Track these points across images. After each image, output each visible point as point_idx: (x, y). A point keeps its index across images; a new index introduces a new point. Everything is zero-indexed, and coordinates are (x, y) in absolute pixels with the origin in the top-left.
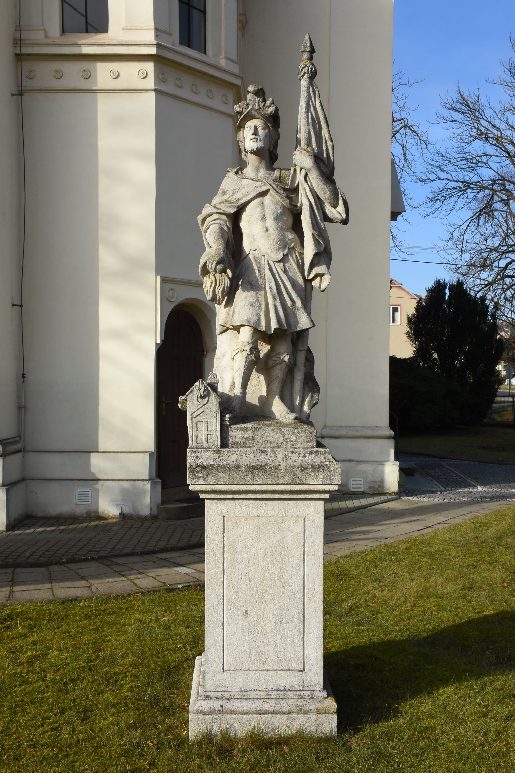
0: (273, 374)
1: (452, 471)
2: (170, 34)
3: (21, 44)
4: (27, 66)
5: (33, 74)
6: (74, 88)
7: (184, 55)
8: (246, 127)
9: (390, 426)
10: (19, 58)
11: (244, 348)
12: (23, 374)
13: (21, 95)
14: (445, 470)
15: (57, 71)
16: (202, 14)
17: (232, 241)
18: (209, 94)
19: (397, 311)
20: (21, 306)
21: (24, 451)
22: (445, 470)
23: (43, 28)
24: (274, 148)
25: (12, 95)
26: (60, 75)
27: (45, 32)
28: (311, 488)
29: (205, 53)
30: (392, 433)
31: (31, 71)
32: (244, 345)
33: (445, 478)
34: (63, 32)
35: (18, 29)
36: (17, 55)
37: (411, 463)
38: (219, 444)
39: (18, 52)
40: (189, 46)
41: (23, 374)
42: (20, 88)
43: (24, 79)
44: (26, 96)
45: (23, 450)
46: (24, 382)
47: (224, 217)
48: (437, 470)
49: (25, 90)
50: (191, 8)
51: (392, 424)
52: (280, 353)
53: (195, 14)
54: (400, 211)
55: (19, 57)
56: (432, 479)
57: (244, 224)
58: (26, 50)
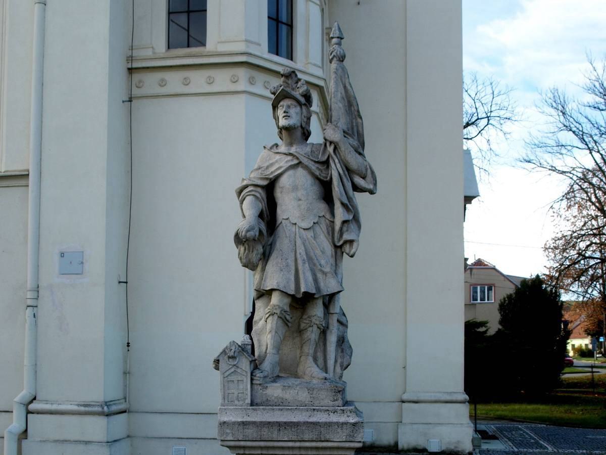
0: (306, 336)
1: (527, 434)
2: (259, 45)
3: (132, 60)
4: (136, 77)
5: (141, 84)
6: (176, 94)
7: (271, 61)
8: (279, 106)
9: (465, 390)
10: (131, 70)
11: (275, 311)
12: (128, 343)
13: (130, 101)
14: (522, 432)
15: (163, 80)
16: (289, 28)
17: (266, 211)
18: (251, 81)
19: (492, 290)
20: (126, 283)
21: (129, 412)
22: (522, 432)
23: (151, 46)
24: (306, 124)
25: (123, 102)
26: (164, 83)
27: (153, 48)
28: (335, 444)
29: (292, 60)
30: (467, 397)
31: (140, 81)
32: (274, 308)
33: (520, 440)
34: (169, 47)
35: (131, 48)
36: (129, 69)
37: (492, 426)
38: (250, 402)
39: (130, 67)
40: (277, 54)
41: (128, 343)
42: (130, 96)
43: (134, 88)
44: (134, 102)
45: (127, 411)
46: (128, 350)
47: (259, 190)
48: (514, 432)
49: (134, 98)
50: (280, 24)
51: (467, 389)
52: (311, 316)
53: (284, 29)
54: (475, 195)
55: (130, 71)
56: (507, 440)
57: (279, 195)
58: (135, 65)
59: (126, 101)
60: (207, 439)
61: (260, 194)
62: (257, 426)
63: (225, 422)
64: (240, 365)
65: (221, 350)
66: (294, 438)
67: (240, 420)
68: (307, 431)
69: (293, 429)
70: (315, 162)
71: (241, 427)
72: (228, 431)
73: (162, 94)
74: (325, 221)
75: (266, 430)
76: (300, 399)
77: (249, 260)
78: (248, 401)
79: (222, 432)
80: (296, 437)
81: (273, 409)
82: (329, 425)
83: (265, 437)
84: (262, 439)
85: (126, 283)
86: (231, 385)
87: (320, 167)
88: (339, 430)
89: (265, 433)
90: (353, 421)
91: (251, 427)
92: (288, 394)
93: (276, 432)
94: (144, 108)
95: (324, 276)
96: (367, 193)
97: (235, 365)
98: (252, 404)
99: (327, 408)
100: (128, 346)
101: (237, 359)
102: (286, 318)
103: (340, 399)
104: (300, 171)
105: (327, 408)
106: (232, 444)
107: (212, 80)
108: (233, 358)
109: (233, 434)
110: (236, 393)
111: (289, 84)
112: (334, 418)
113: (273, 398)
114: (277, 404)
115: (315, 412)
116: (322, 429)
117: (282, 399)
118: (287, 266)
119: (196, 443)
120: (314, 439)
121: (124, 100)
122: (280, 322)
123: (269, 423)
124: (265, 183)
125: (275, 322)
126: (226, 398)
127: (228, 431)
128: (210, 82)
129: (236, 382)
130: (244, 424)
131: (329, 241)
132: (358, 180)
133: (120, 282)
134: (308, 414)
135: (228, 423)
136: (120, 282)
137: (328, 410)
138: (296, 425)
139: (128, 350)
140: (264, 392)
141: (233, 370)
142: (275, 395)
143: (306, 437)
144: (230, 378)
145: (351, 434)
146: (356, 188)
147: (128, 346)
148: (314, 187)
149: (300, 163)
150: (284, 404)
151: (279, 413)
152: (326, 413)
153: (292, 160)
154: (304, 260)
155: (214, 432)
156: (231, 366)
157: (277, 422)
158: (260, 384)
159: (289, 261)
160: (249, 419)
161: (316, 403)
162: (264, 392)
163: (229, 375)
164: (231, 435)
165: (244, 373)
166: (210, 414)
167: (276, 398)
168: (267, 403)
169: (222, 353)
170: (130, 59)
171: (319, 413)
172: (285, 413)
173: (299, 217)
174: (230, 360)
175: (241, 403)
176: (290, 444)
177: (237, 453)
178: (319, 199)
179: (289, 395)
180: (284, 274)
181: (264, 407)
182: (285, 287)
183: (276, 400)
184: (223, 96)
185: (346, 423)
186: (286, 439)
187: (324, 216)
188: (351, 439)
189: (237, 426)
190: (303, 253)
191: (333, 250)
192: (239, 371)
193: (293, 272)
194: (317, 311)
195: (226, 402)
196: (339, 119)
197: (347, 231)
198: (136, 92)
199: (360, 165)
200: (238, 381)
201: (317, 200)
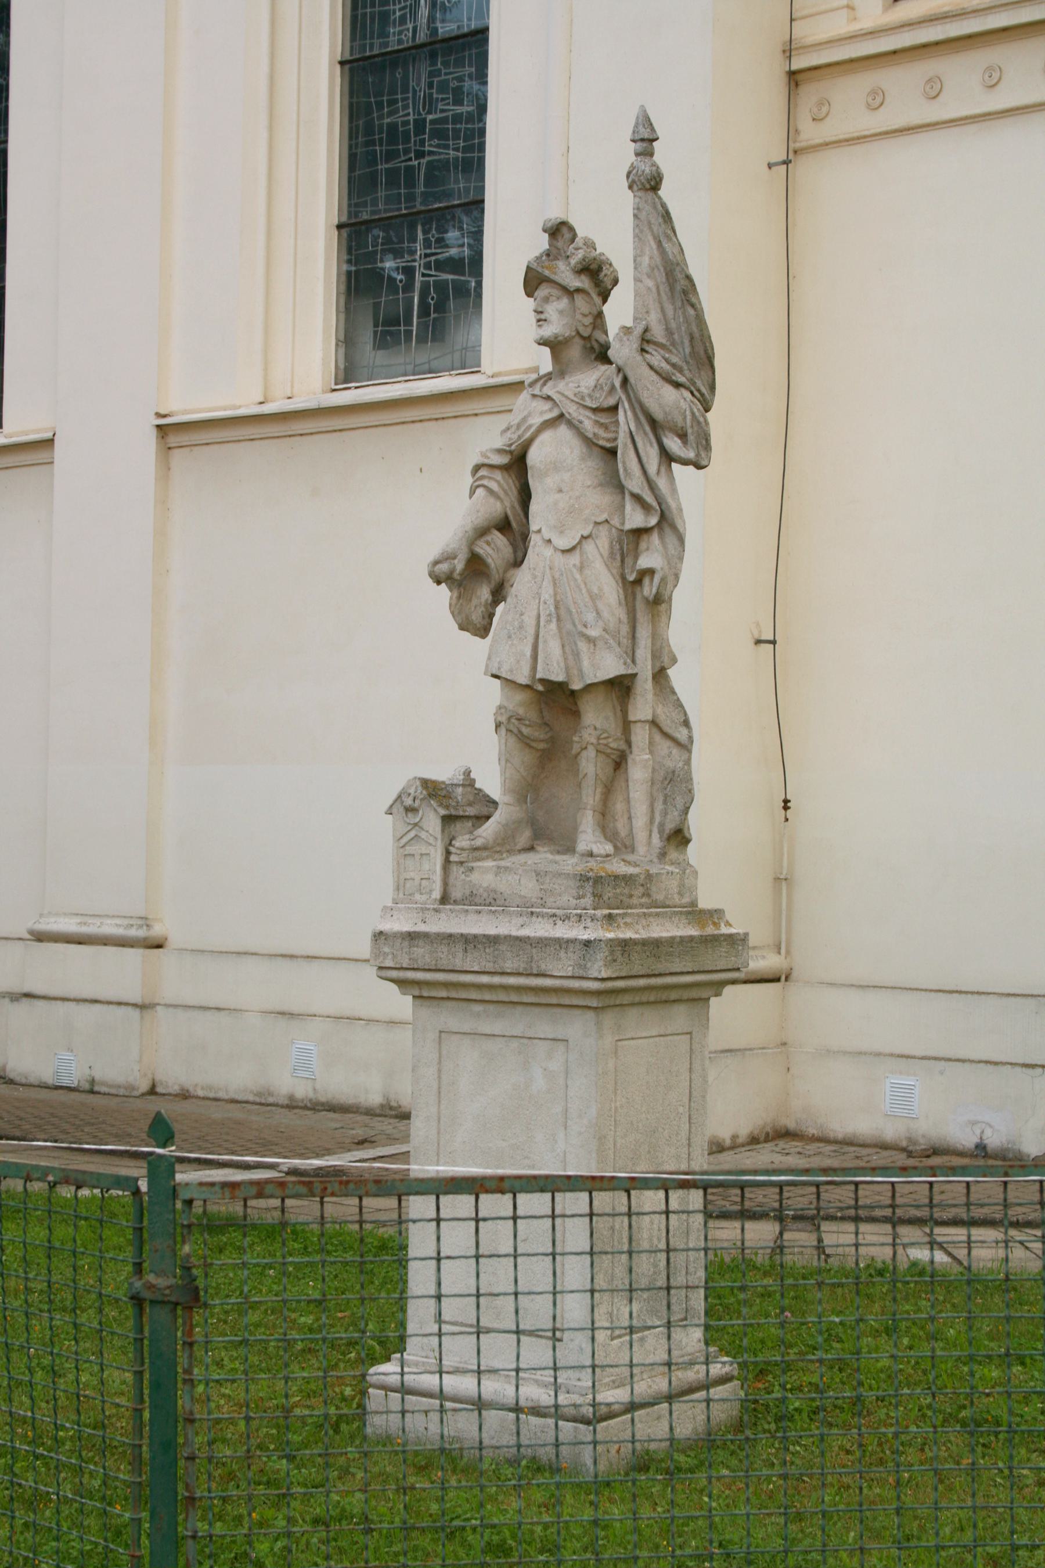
5: (825, 109)
10: (794, 78)
12: (786, 801)
20: (773, 642)
25: (770, 166)
28: (557, 983)
38: (438, 897)
41: (786, 801)
46: (787, 820)
58: (799, 63)
59: (777, 164)
60: (914, 1057)
61: (498, 482)
62: (432, 942)
63: (381, 933)
64: (424, 824)
65: (394, 796)
66: (490, 967)
67: (407, 927)
68: (509, 954)
69: (487, 950)
70: (595, 410)
71: (406, 943)
72: (386, 950)
73: (872, 131)
74: (610, 531)
75: (445, 949)
76: (522, 893)
77: (467, 618)
78: (437, 894)
79: (377, 953)
80: (491, 964)
81: (467, 911)
82: (543, 943)
83: (444, 964)
84: (439, 967)
85: (773, 642)
86: (409, 862)
87: (602, 421)
88: (562, 954)
89: (444, 956)
90: (585, 937)
91: (421, 943)
92: (504, 882)
93: (460, 955)
94: (826, 179)
95: (592, 645)
96: (691, 467)
97: (416, 825)
98: (444, 899)
99: (554, 911)
100: (786, 808)
101: (421, 812)
102: (520, 732)
103: (589, 895)
104: (563, 430)
105: (554, 911)
106: (394, 974)
107: (996, 75)
108: (410, 810)
109: (394, 956)
110: (417, 878)
111: (558, 249)
112: (562, 931)
113: (481, 890)
114: (487, 902)
115: (534, 918)
116: (534, 951)
117: (495, 891)
118: (521, 627)
119: (942, 1073)
120: (521, 970)
121: (773, 161)
122: (512, 740)
123: (450, 936)
124: (504, 460)
125: (503, 741)
126: (401, 888)
127: (386, 950)
128: (934, 91)
129: (417, 857)
130: (412, 937)
131: (612, 575)
132: (673, 444)
133: (758, 642)
134: (521, 920)
135: (386, 934)
136: (758, 642)
137: (554, 915)
138: (493, 940)
139: (787, 820)
140: (468, 879)
141: (412, 834)
142: (485, 885)
143: (509, 966)
144: (409, 849)
145: (582, 962)
146: (667, 457)
147: (786, 808)
148: (589, 463)
149: (562, 416)
150: (498, 902)
151: (475, 917)
152: (551, 920)
153: (551, 410)
154: (550, 615)
155: (364, 948)
156: (410, 827)
157: (462, 935)
158: (462, 863)
159: (525, 618)
160: (422, 928)
161: (550, 901)
162: (468, 879)
163: (406, 844)
164: (390, 956)
165: (431, 840)
166: (960, 992)
167: (486, 889)
168: (472, 900)
169: (396, 801)
170: (789, 51)
171: (540, 919)
172: (484, 919)
173: (555, 527)
174: (410, 815)
175: (424, 897)
176: (485, 979)
177: (417, 993)
178: (601, 485)
179: (505, 884)
180: (512, 644)
181: (466, 907)
182: (511, 671)
183: (485, 895)
184: (988, 123)
185: (574, 941)
186: (476, 968)
187: (607, 521)
188: (581, 973)
189: (399, 940)
190: (551, 602)
191: (621, 591)
192: (423, 835)
193: (530, 640)
194: (596, 718)
195: (401, 895)
196: (647, 312)
197: (647, 549)
198: (810, 133)
199: (667, 409)
200: (422, 855)
201: (595, 488)
